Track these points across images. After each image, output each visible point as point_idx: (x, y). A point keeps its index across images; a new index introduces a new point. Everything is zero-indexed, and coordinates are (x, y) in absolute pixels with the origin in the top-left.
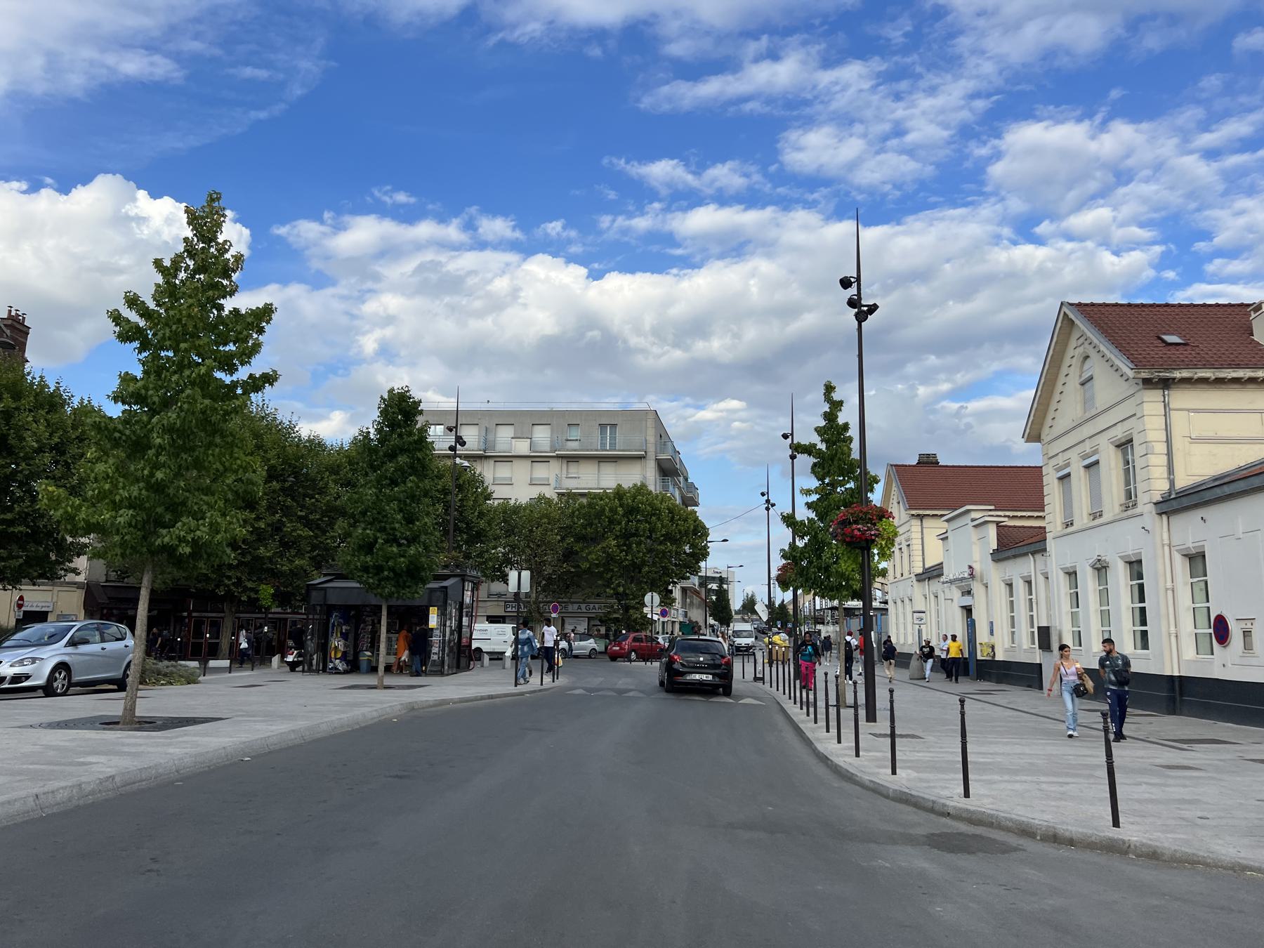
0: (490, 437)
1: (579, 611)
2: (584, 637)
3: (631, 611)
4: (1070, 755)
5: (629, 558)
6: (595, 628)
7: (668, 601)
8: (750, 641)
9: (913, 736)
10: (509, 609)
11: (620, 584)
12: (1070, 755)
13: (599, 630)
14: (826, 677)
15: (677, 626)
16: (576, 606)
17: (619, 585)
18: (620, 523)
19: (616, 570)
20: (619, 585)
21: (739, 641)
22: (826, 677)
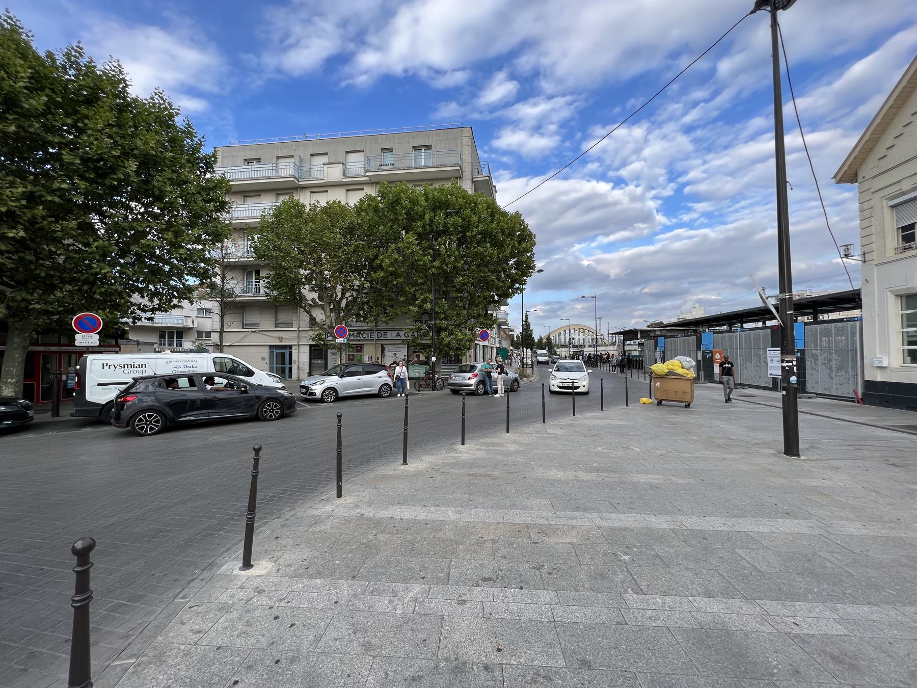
0: (306, 168)
1: (398, 338)
2: (66, 277)
3: (443, 334)
4: (812, 393)
5: (437, 263)
6: (415, 354)
7: (489, 322)
8: (546, 358)
9: (911, 123)
10: (352, 338)
11: (428, 300)
12: (812, 393)
13: (419, 357)
14: (339, 421)
15: (495, 351)
16: (395, 333)
17: (425, 300)
18: (422, 217)
19: (421, 281)
20: (425, 300)
21: (540, 359)
22: (339, 421)
